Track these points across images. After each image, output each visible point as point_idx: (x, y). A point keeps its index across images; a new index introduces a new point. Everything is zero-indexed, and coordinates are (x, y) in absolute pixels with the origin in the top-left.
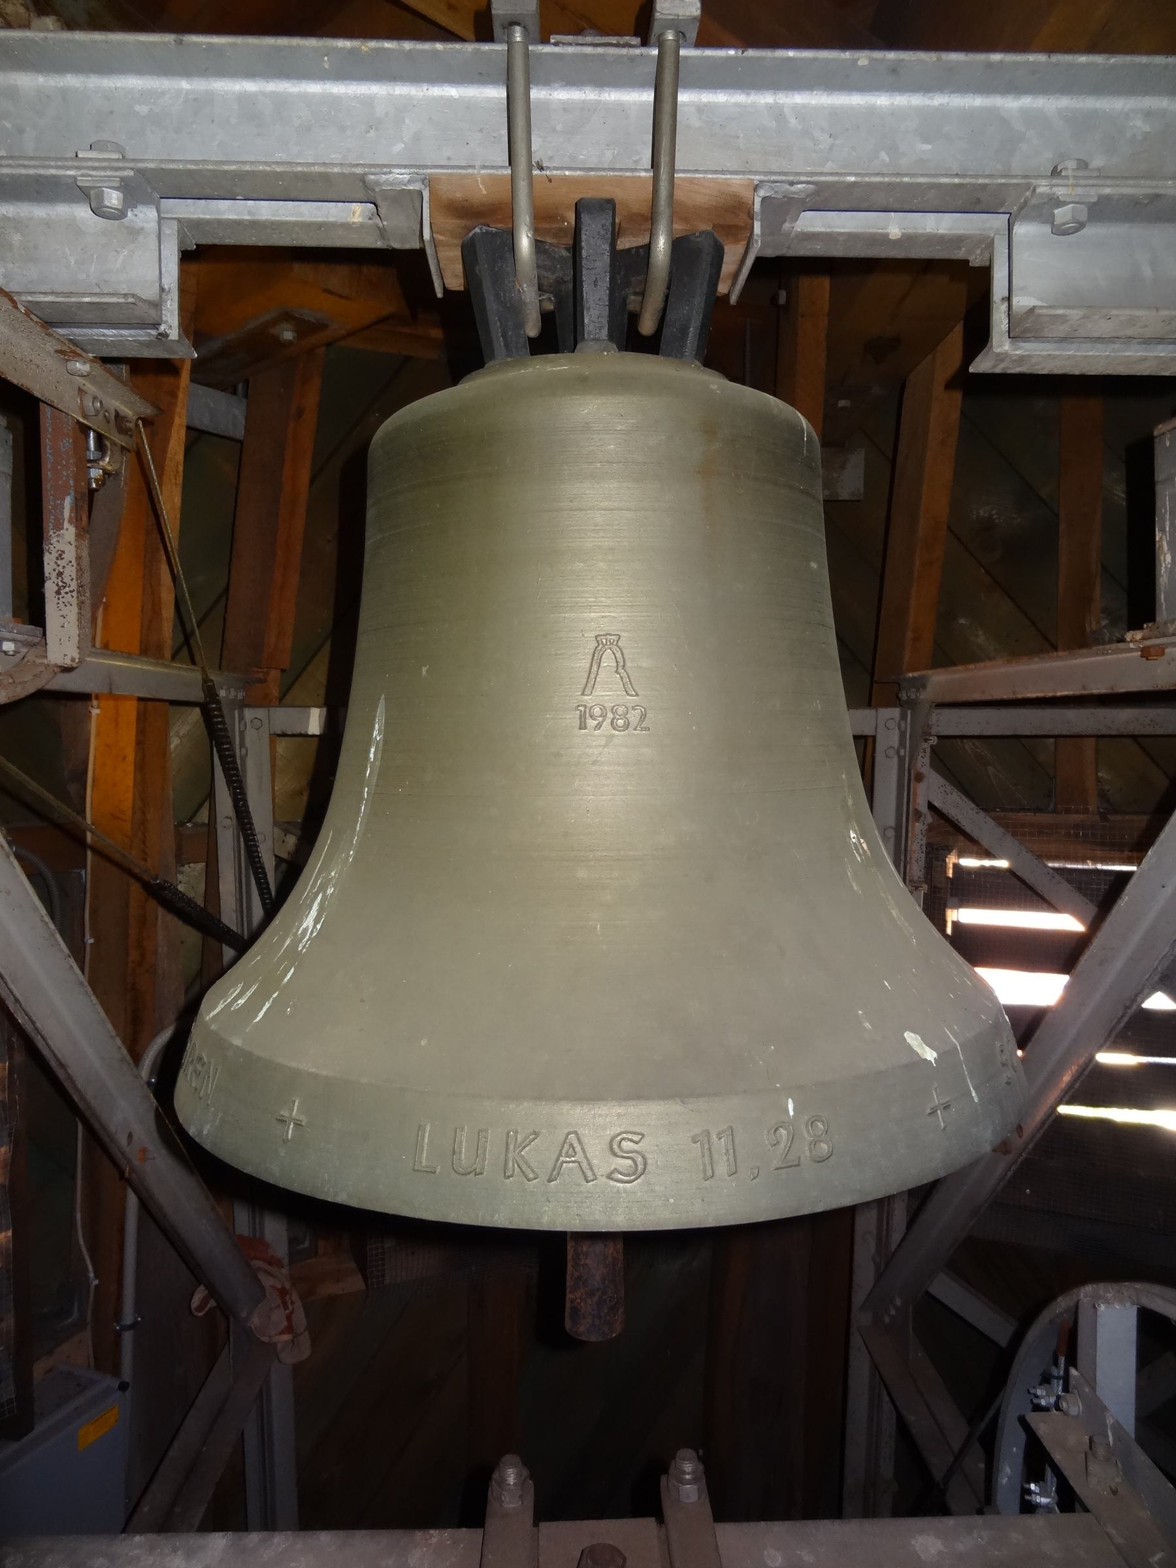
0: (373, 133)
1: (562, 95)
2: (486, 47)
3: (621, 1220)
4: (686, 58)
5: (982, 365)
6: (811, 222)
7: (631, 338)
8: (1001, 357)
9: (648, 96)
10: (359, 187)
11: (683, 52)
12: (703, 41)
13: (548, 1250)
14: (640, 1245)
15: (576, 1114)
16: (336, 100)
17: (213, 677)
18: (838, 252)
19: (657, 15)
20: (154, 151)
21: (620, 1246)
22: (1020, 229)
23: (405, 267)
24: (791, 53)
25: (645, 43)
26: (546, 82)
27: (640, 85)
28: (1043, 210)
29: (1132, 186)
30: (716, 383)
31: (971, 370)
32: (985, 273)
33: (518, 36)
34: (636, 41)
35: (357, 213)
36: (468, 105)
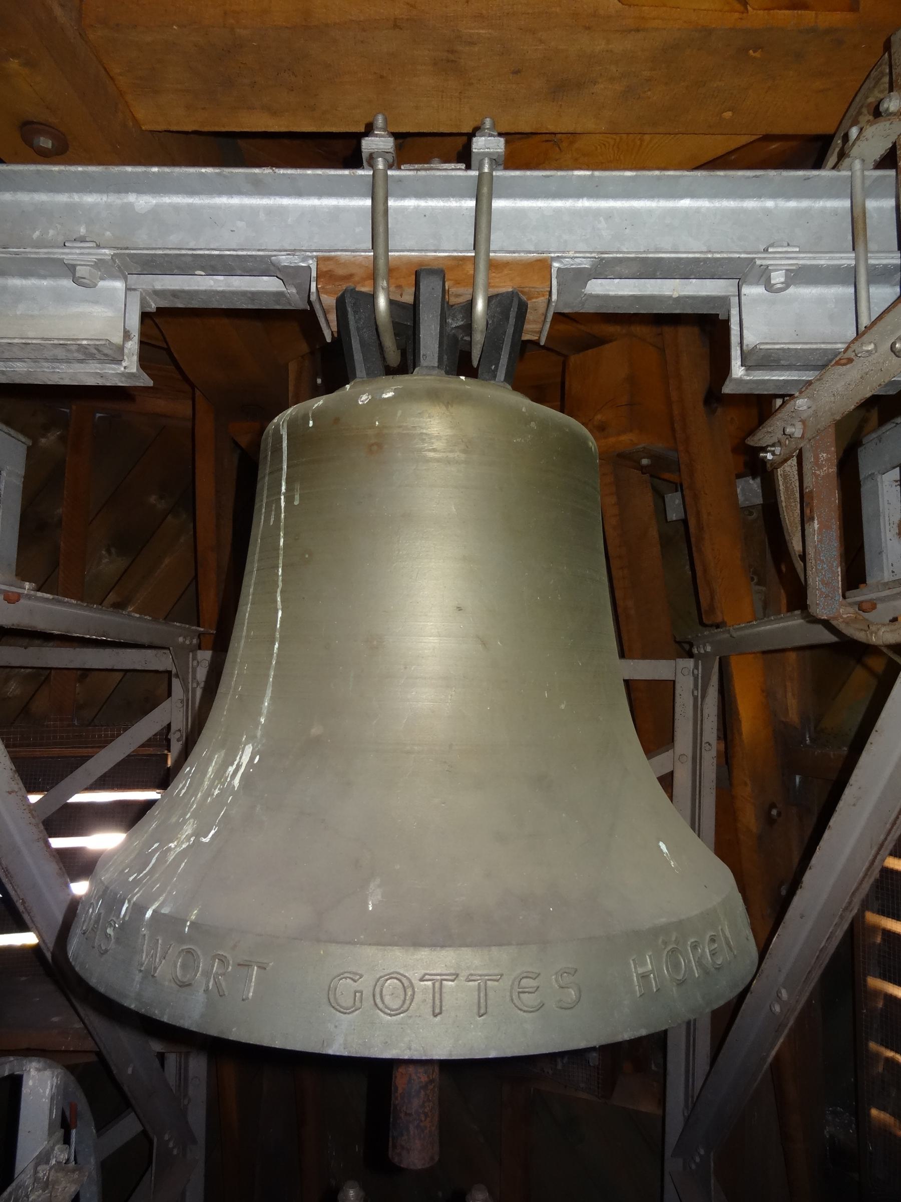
0: (281, 227)
1: (410, 203)
2: (360, 172)
3: (442, 1051)
4: (497, 176)
5: (727, 389)
6: (597, 287)
7: (460, 362)
8: (740, 381)
9: (472, 203)
10: (261, 266)
11: (494, 173)
12: (507, 168)
13: (378, 1074)
14: (454, 1071)
15: (398, 959)
16: (522, 212)
17: (795, 622)
18: (195, 304)
19: (363, 150)
20: (145, 241)
21: (437, 1069)
22: (745, 290)
23: (304, 319)
24: (129, 169)
25: (468, 167)
26: (500, 197)
27: (362, 195)
28: (763, 277)
29: (56, 253)
30: (524, 403)
31: (150, 383)
32: (726, 323)
33: (381, 165)
34: (463, 166)
35: (269, 284)
36: (448, 213)
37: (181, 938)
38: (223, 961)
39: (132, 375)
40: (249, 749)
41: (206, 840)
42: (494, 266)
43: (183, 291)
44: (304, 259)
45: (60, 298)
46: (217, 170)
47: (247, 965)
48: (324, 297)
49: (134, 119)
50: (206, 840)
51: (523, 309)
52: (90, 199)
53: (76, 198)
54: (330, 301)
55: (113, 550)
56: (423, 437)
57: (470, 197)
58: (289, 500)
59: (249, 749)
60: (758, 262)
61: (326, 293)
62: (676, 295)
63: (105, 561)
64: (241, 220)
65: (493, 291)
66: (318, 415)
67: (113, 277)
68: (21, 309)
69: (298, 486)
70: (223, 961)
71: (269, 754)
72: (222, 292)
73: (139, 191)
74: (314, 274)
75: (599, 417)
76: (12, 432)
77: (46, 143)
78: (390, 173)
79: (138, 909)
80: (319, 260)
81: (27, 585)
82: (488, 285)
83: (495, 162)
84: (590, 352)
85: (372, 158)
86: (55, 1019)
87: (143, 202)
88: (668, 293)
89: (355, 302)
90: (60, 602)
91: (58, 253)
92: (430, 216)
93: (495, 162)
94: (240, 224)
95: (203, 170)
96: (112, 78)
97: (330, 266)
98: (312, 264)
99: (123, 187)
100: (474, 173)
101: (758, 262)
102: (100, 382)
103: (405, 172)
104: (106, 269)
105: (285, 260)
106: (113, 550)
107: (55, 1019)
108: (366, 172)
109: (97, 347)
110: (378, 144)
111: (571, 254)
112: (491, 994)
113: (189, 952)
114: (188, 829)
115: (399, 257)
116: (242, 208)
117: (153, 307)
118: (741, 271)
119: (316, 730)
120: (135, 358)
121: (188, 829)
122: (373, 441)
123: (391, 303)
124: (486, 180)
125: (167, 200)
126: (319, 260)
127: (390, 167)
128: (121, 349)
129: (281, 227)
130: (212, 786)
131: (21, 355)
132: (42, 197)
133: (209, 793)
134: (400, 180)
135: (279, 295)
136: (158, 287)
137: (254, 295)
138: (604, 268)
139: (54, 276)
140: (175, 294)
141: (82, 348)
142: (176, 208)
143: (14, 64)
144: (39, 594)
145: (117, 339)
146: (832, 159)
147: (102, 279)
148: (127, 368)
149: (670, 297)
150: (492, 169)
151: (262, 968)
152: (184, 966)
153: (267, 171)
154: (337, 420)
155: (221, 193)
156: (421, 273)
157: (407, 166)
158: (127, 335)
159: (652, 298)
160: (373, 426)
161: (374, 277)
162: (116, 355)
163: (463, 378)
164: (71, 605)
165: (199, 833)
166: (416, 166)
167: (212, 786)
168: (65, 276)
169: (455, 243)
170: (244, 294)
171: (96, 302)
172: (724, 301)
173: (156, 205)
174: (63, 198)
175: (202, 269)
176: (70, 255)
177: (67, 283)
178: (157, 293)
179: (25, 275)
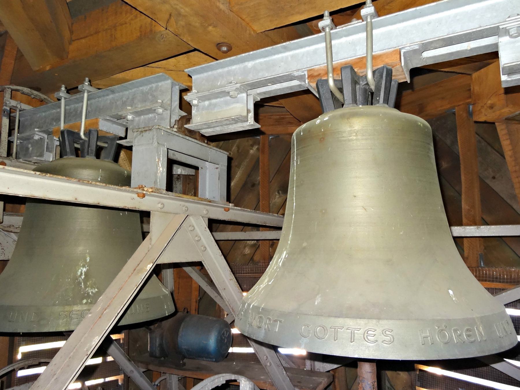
0: (294, 62)
1: (344, 40)
2: (320, 34)
6: (427, 54)
7: (370, 98)
8: (507, 81)
9: (365, 34)
10: (290, 78)
12: (379, 16)
20: (252, 78)
24: (243, 55)
25: (363, 21)
28: (506, 32)
34: (361, 21)
35: (295, 83)
37: (259, 313)
38: (270, 319)
39: (252, 125)
40: (285, 252)
41: (270, 283)
42: (374, 58)
43: (267, 92)
44: (303, 72)
45: (227, 103)
46: (271, 47)
47: (276, 321)
48: (311, 84)
49: (254, 30)
50: (270, 283)
51: (389, 73)
52: (234, 67)
53: (230, 68)
54: (314, 85)
55: (280, 192)
56: (345, 132)
57: (364, 32)
58: (297, 163)
59: (285, 252)
60: (501, 27)
61: (312, 82)
62: (469, 48)
63: (277, 197)
64: (282, 62)
65: (375, 68)
66: (304, 130)
67: (242, 92)
68: (216, 110)
69: (299, 157)
70: (270, 319)
71: (290, 253)
72: (280, 89)
73: (248, 61)
74: (307, 76)
75: (489, 102)
76: (221, 151)
77: (224, 49)
78: (332, 31)
79: (249, 305)
80: (308, 71)
81: (231, 204)
82: (373, 66)
83: (373, 16)
84: (482, 70)
85: (324, 29)
86: (262, 377)
87: (250, 64)
88: (466, 48)
89: (322, 83)
90: (244, 211)
91: (223, 89)
92: (349, 44)
93: (373, 16)
94: (282, 64)
95: (267, 49)
96: (243, 20)
97: (312, 72)
98: (306, 73)
99: (243, 61)
100: (365, 22)
101: (501, 27)
102: (244, 129)
103: (339, 29)
104: (239, 90)
105: (296, 74)
106: (280, 192)
107: (262, 377)
108: (323, 34)
109: (237, 118)
110: (327, 21)
111: (408, 45)
112: (356, 335)
113: (261, 317)
114: (266, 281)
115: (337, 63)
116: (283, 57)
117: (259, 99)
118: (495, 31)
119: (305, 244)
120: (253, 119)
121: (266, 281)
122: (321, 137)
123: (335, 81)
124: (369, 24)
125: (258, 61)
126: (308, 71)
127: (332, 29)
128: (247, 117)
129: (294, 62)
130: (274, 266)
131: (216, 125)
132: (220, 71)
133: (273, 269)
134: (336, 33)
135: (300, 85)
136: (258, 92)
137: (291, 88)
138: (426, 46)
139: (224, 96)
140: (265, 93)
141: (233, 119)
142: (261, 63)
143: (210, 28)
144: (236, 208)
145: (245, 114)
146: (86, 154)
147: (238, 94)
148: (250, 123)
149: (467, 50)
150: (371, 19)
151: (280, 322)
152: (259, 321)
153: (288, 43)
154: (309, 131)
155: (274, 54)
156: (350, 67)
157: (339, 27)
158: (248, 111)
159: (458, 52)
160: (321, 131)
161: (327, 73)
162: (245, 119)
163: (361, 106)
164: (249, 212)
165: (268, 281)
166: (343, 26)
167: (274, 266)
168: (227, 96)
169: (361, 52)
170: (287, 88)
171: (238, 102)
172: (496, 45)
173: (255, 64)
174: (226, 69)
175: (270, 83)
176: (227, 89)
177: (228, 98)
178: (259, 94)
179: (216, 98)
